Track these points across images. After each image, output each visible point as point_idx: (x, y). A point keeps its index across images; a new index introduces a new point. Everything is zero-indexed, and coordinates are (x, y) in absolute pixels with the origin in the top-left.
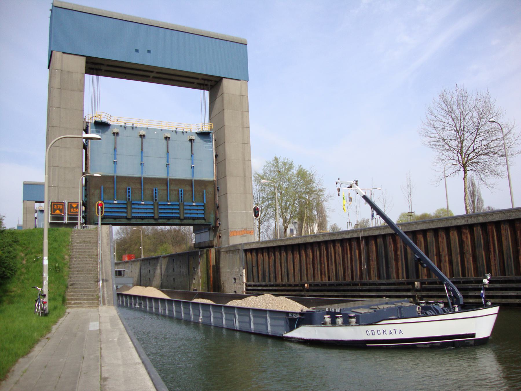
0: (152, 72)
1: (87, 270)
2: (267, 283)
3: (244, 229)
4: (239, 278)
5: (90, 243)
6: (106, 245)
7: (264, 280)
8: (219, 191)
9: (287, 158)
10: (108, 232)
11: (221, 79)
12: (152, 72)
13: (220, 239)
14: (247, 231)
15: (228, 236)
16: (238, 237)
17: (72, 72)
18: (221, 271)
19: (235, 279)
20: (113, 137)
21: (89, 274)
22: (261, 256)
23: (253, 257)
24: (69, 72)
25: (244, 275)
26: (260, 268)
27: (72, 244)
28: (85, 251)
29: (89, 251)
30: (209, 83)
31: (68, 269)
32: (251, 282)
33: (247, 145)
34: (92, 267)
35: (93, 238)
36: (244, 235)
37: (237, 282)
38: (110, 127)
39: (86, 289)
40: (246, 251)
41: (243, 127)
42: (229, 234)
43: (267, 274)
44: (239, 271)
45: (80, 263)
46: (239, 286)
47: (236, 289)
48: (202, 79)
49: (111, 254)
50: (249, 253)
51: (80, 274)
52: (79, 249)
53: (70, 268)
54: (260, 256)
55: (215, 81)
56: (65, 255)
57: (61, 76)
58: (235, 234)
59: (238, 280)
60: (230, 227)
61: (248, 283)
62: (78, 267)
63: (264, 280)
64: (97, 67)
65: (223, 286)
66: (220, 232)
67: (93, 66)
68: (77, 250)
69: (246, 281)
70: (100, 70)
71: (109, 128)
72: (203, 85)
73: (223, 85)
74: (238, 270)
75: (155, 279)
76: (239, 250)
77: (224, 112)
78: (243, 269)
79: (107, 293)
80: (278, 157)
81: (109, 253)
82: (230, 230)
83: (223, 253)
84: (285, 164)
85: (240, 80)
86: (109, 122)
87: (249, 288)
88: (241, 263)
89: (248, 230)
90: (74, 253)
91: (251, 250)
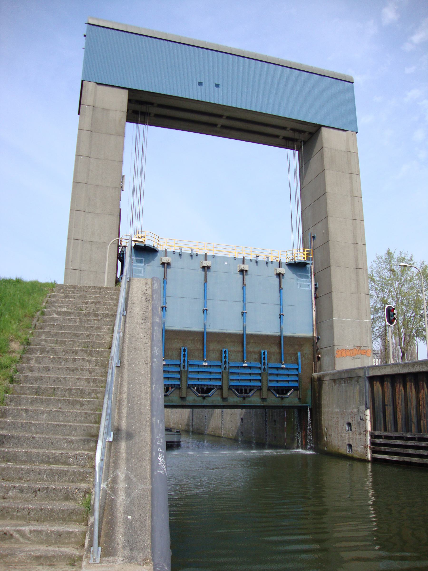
0: (220, 116)
1: (71, 390)
2: (414, 433)
3: (358, 347)
4: (359, 423)
5: (97, 315)
6: (140, 321)
7: (408, 429)
8: (317, 290)
9: (404, 252)
10: (149, 292)
11: (318, 128)
12: (220, 116)
13: (319, 362)
14: (361, 350)
15: (333, 357)
16: (348, 359)
17: (109, 110)
18: (323, 411)
19: (349, 424)
20: (162, 269)
21: (74, 403)
22: (402, 388)
23: (386, 390)
24: (104, 109)
25: (368, 418)
26: (400, 408)
27: (43, 313)
28: (75, 334)
29: (88, 336)
30: (302, 137)
31: (7, 381)
32: (381, 431)
33: (359, 221)
34: (88, 381)
35: (105, 304)
36: (357, 356)
37: (353, 429)
38: (158, 254)
39: (49, 463)
40: (372, 379)
41: (353, 196)
42: (335, 354)
43: (414, 419)
44: (358, 411)
45: (51, 366)
46: (358, 437)
47: (351, 440)
48: (292, 129)
49: (152, 347)
50: (378, 383)
51: (42, 402)
52: (61, 328)
53: (12, 381)
54: (400, 388)
55: (310, 133)
56: (12, 341)
57: (93, 114)
58: (344, 354)
59: (356, 426)
60: (336, 342)
61: (377, 433)
62: (41, 378)
63: (408, 429)
64: (144, 108)
65: (326, 435)
66: (318, 351)
67: (138, 107)
68: (54, 331)
69: (371, 430)
70: (149, 114)
71: (156, 255)
72: (293, 140)
73: (322, 135)
74: (355, 410)
75: (213, 418)
76: (359, 377)
77: (324, 174)
78: (367, 408)
79: (128, 492)
80: (392, 251)
81: (148, 342)
82: (336, 347)
83: (327, 382)
84: (402, 260)
85: (345, 131)
86: (156, 246)
87: (378, 441)
88: (363, 400)
89: (362, 348)
90: (43, 337)
91: (382, 379)
